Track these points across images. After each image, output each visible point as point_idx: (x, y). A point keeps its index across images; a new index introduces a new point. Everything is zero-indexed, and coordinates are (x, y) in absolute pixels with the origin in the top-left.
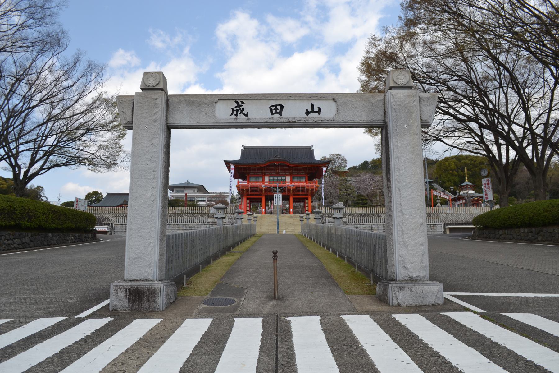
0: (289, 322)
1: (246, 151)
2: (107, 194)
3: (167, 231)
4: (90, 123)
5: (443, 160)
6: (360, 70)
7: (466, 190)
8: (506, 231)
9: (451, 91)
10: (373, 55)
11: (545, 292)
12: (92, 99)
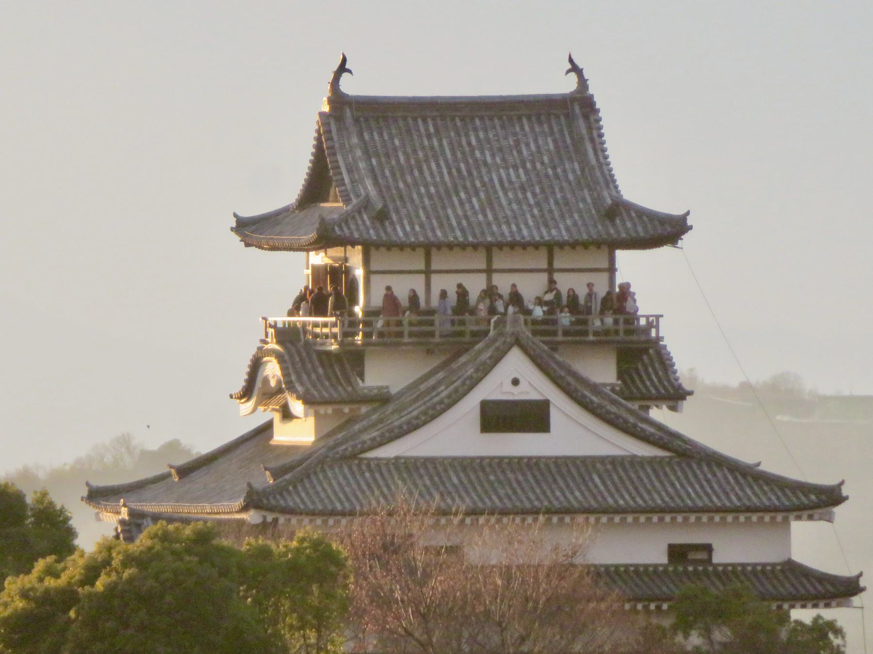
0: (360, 269)
1: (433, 315)
2: (356, 247)
3: (336, 330)
4: (321, 476)
5: (458, 300)
6: (220, 544)
7: (47, 591)
8: (651, 232)
9: (574, 197)
10: (393, 434)
11: (345, 283)
12: (588, 80)
